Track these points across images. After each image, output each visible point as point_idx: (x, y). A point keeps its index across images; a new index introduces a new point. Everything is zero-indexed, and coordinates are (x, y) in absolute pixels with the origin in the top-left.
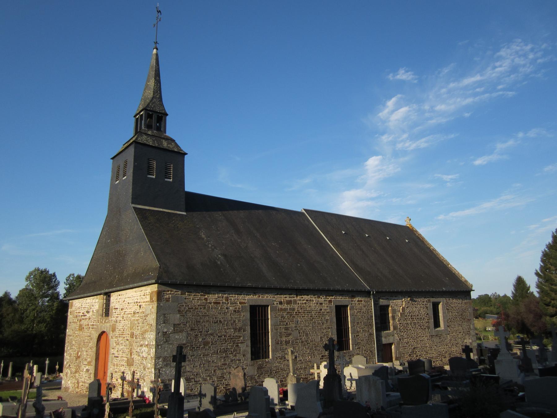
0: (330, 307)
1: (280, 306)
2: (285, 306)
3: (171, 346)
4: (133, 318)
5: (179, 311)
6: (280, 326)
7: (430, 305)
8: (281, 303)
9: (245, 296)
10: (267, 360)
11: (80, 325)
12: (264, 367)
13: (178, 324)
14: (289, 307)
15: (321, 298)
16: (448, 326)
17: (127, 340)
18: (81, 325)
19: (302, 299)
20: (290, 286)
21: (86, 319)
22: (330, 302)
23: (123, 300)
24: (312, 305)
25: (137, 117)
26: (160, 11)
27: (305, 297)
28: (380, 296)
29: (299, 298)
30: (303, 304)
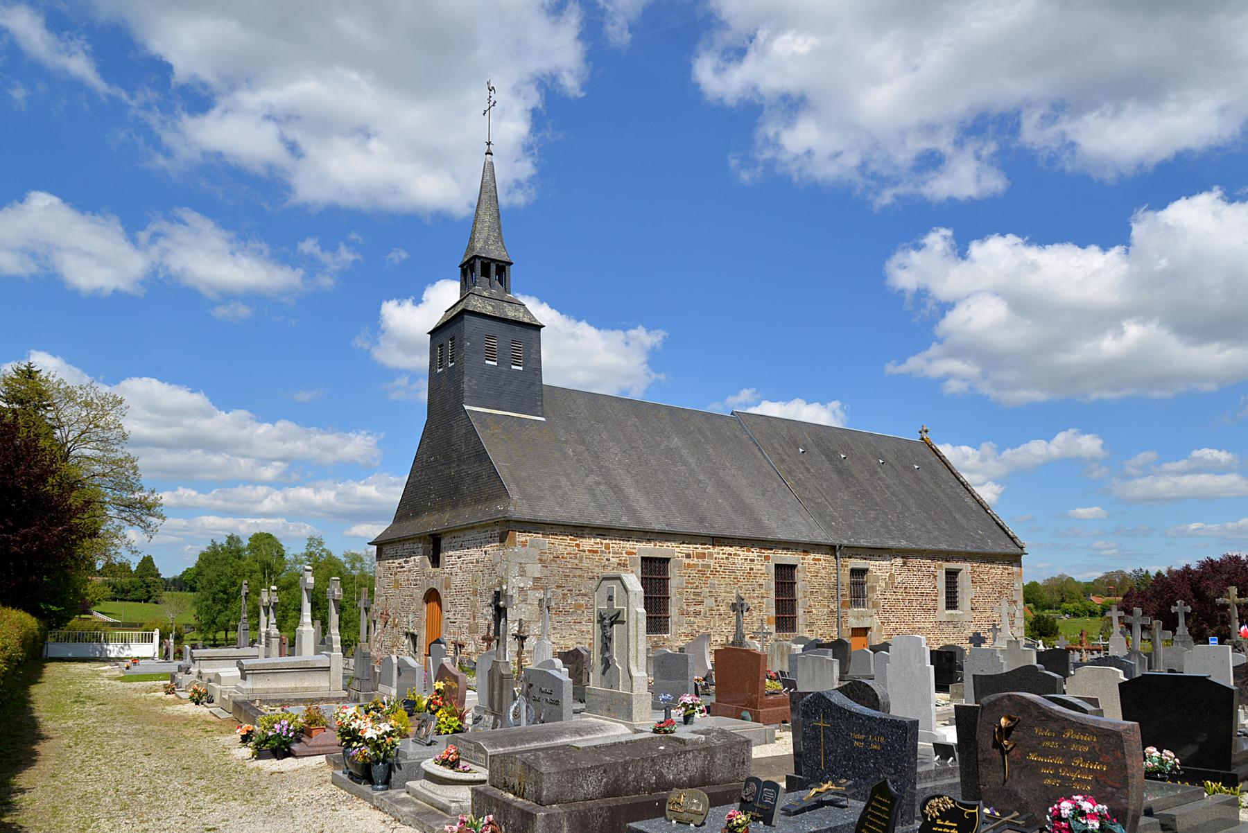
0: (767, 566)
1: (687, 561)
2: (695, 561)
3: (530, 607)
4: (476, 569)
5: (541, 560)
6: (687, 590)
7: (942, 572)
8: (688, 556)
9: (635, 543)
10: (665, 636)
11: (395, 580)
12: (660, 646)
13: (539, 578)
14: (701, 562)
15: (753, 552)
16: (972, 609)
17: (468, 599)
18: (396, 581)
19: (721, 552)
20: (703, 531)
21: (404, 571)
22: (767, 558)
23: (460, 543)
24: (739, 561)
25: (465, 267)
26: (493, 88)
27: (727, 549)
28: (853, 554)
29: (717, 549)
30: (722, 559)
